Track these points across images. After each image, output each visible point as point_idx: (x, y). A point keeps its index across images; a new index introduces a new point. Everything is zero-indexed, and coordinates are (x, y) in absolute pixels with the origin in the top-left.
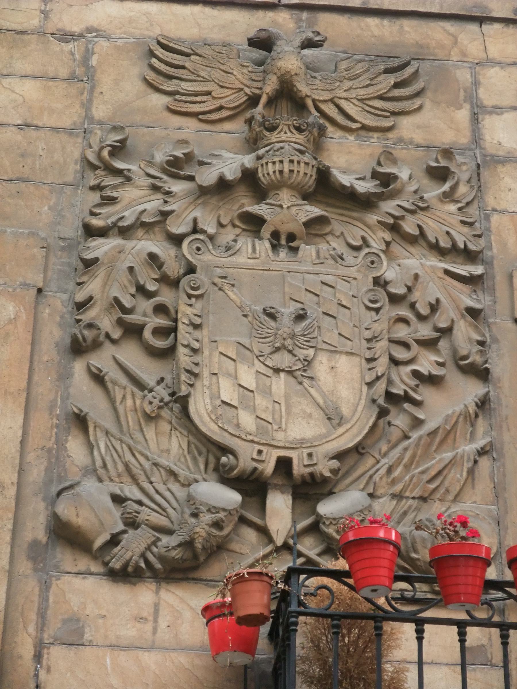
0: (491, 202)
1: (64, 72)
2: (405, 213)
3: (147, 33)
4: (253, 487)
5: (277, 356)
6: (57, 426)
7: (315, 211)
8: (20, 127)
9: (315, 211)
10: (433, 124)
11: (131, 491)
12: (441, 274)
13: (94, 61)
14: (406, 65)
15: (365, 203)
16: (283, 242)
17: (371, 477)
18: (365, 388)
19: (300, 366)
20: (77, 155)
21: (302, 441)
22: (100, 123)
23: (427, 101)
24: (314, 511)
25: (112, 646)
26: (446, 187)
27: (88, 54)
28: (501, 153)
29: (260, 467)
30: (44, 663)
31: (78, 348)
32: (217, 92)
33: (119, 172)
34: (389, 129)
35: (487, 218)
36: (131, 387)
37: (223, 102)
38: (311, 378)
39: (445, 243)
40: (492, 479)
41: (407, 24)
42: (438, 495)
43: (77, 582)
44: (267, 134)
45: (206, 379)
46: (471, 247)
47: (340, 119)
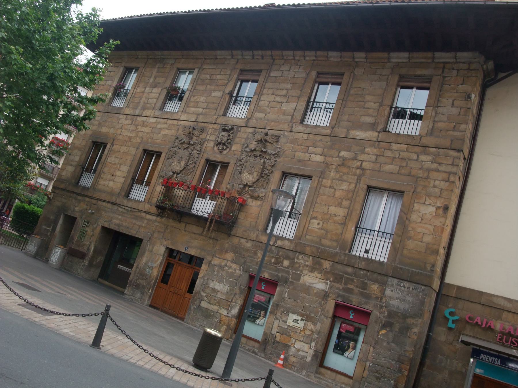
10: (203, 136)
15: (193, 145)
31: (168, 159)
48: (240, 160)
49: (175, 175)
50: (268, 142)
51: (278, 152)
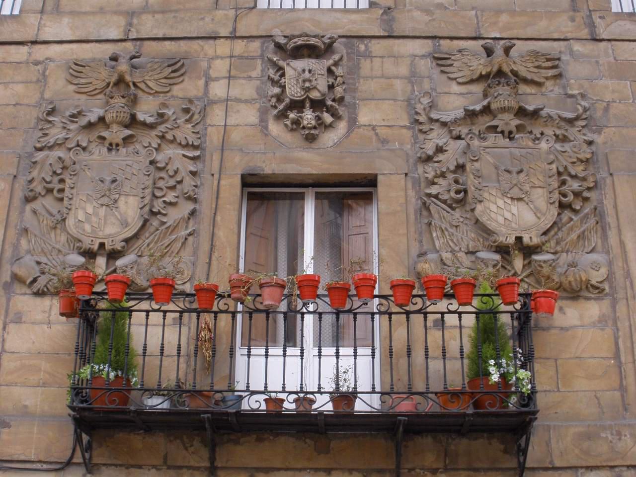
0: (208, 121)
1: (34, 79)
2: (168, 130)
3: (70, 58)
4: (90, 255)
5: (102, 199)
6: (17, 234)
7: (128, 132)
8: (14, 105)
9: (128, 132)
10: (190, 87)
11: (43, 260)
12: (181, 156)
13: (47, 73)
14: (180, 61)
15: (151, 126)
16: (114, 147)
17: (140, 248)
18: (139, 210)
19: (112, 202)
20: (36, 116)
21: (110, 235)
22: (47, 100)
23: (186, 78)
24: (115, 265)
25: (33, 323)
26: (188, 117)
27: (45, 70)
28: (216, 99)
29: (92, 247)
30: (6, 331)
31: (28, 200)
32: (95, 82)
33: (50, 122)
34: (168, 92)
35: (206, 129)
36: (47, 215)
37: (97, 87)
38: (117, 208)
39: (184, 143)
40: (193, 245)
41: (182, 43)
42: (168, 254)
43: (22, 298)
44: (110, 100)
45: (73, 212)
46: (195, 144)
47: (147, 90)
48: (429, 159)
49: (101, 261)
50: (525, 81)
51: (585, 110)
